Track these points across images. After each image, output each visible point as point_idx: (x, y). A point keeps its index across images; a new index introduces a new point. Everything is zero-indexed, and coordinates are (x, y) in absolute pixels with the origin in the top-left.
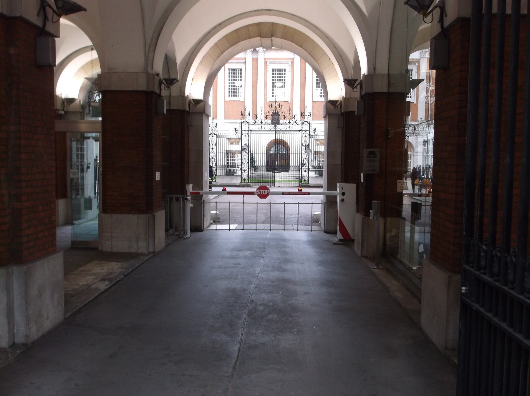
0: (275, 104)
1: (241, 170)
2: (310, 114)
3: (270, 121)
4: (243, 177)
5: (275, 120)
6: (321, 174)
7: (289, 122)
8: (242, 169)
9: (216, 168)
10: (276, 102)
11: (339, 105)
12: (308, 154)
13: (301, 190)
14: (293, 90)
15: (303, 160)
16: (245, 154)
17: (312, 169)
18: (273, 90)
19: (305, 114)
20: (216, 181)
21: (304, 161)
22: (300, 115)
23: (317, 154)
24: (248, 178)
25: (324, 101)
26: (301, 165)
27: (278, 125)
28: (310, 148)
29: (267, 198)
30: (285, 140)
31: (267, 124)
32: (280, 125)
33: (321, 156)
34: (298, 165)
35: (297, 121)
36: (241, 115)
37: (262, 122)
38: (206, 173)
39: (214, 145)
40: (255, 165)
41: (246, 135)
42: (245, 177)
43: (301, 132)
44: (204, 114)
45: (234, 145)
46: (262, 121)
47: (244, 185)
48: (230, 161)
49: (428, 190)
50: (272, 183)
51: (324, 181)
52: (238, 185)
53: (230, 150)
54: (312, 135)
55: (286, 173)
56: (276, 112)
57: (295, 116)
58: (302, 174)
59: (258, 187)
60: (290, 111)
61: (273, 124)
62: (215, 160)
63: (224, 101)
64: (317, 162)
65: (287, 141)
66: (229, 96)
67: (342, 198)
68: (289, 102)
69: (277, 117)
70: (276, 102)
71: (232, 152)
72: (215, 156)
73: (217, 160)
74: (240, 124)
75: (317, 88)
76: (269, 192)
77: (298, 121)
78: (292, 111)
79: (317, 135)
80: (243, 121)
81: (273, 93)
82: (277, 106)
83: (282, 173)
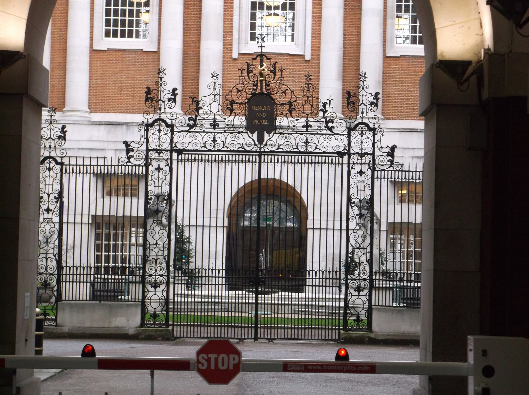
0: (262, 65)
1: (143, 282)
2: (377, 99)
3: (240, 121)
4: (150, 308)
5: (260, 118)
6: (411, 299)
7: (307, 126)
8: (148, 279)
9: (59, 275)
10: (265, 59)
11: (474, 77)
12: (369, 232)
13: (346, 357)
14: (320, 17)
15: (353, 252)
16: (157, 229)
17: (383, 284)
18: (253, 16)
19: (361, 98)
20: (56, 320)
21: (356, 257)
22: (343, 102)
23: (397, 231)
24: (167, 311)
25: (423, 54)
26: (343, 269)
27: (269, 133)
28: (376, 210)
29: (210, 385)
30: (291, 182)
31: (232, 129)
32: (276, 136)
33: (412, 237)
34: (337, 267)
35: (332, 121)
36: (147, 99)
37: (215, 125)
38: (28, 294)
39: (52, 197)
40: (192, 266)
41: (163, 164)
42: (155, 305)
43: (346, 158)
44: (24, 98)
45: (128, 200)
46: (215, 121)
47: (153, 333)
48: (115, 251)
49: (242, 224)
50: (248, 327)
51: (423, 326)
52: (131, 332)
53: (106, 213)
54: (383, 168)
55: (295, 295)
56: (264, 91)
57: (324, 106)
58: (349, 297)
59: (206, 340)
60: (308, 90)
61: (252, 133)
62: (56, 250)
63: (87, 51)
64: (398, 259)
65: (298, 190)
66: (107, 34)
67: (483, 385)
68: (308, 57)
69: (266, 108)
70: (265, 59)
71: (113, 221)
72: (56, 236)
73: (64, 247)
74: (144, 128)
75: (400, 14)
76: (239, 362)
77: (335, 121)
78: (317, 89)
79: (399, 168)
80: (151, 118)
81: (253, 26)
82: (266, 72)
83: (282, 294)
